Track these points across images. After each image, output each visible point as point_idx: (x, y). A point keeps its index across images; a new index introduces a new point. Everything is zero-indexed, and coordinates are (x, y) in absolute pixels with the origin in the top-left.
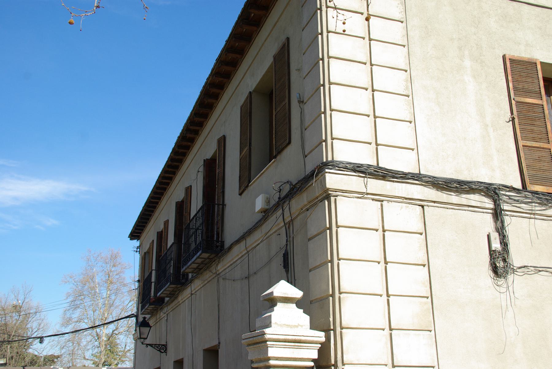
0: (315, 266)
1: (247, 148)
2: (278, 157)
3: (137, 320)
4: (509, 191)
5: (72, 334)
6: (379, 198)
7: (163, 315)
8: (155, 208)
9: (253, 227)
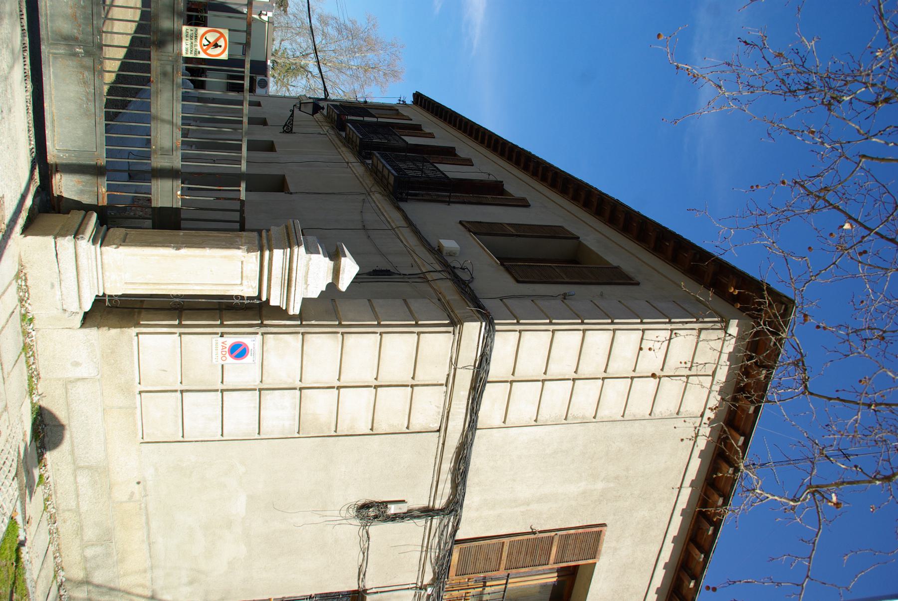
0: (374, 305)
1: (514, 232)
2: (501, 268)
3: (321, 99)
4: (453, 526)
5: (309, 26)
6: (450, 382)
7: (325, 129)
8: (449, 123)
9: (423, 237)
